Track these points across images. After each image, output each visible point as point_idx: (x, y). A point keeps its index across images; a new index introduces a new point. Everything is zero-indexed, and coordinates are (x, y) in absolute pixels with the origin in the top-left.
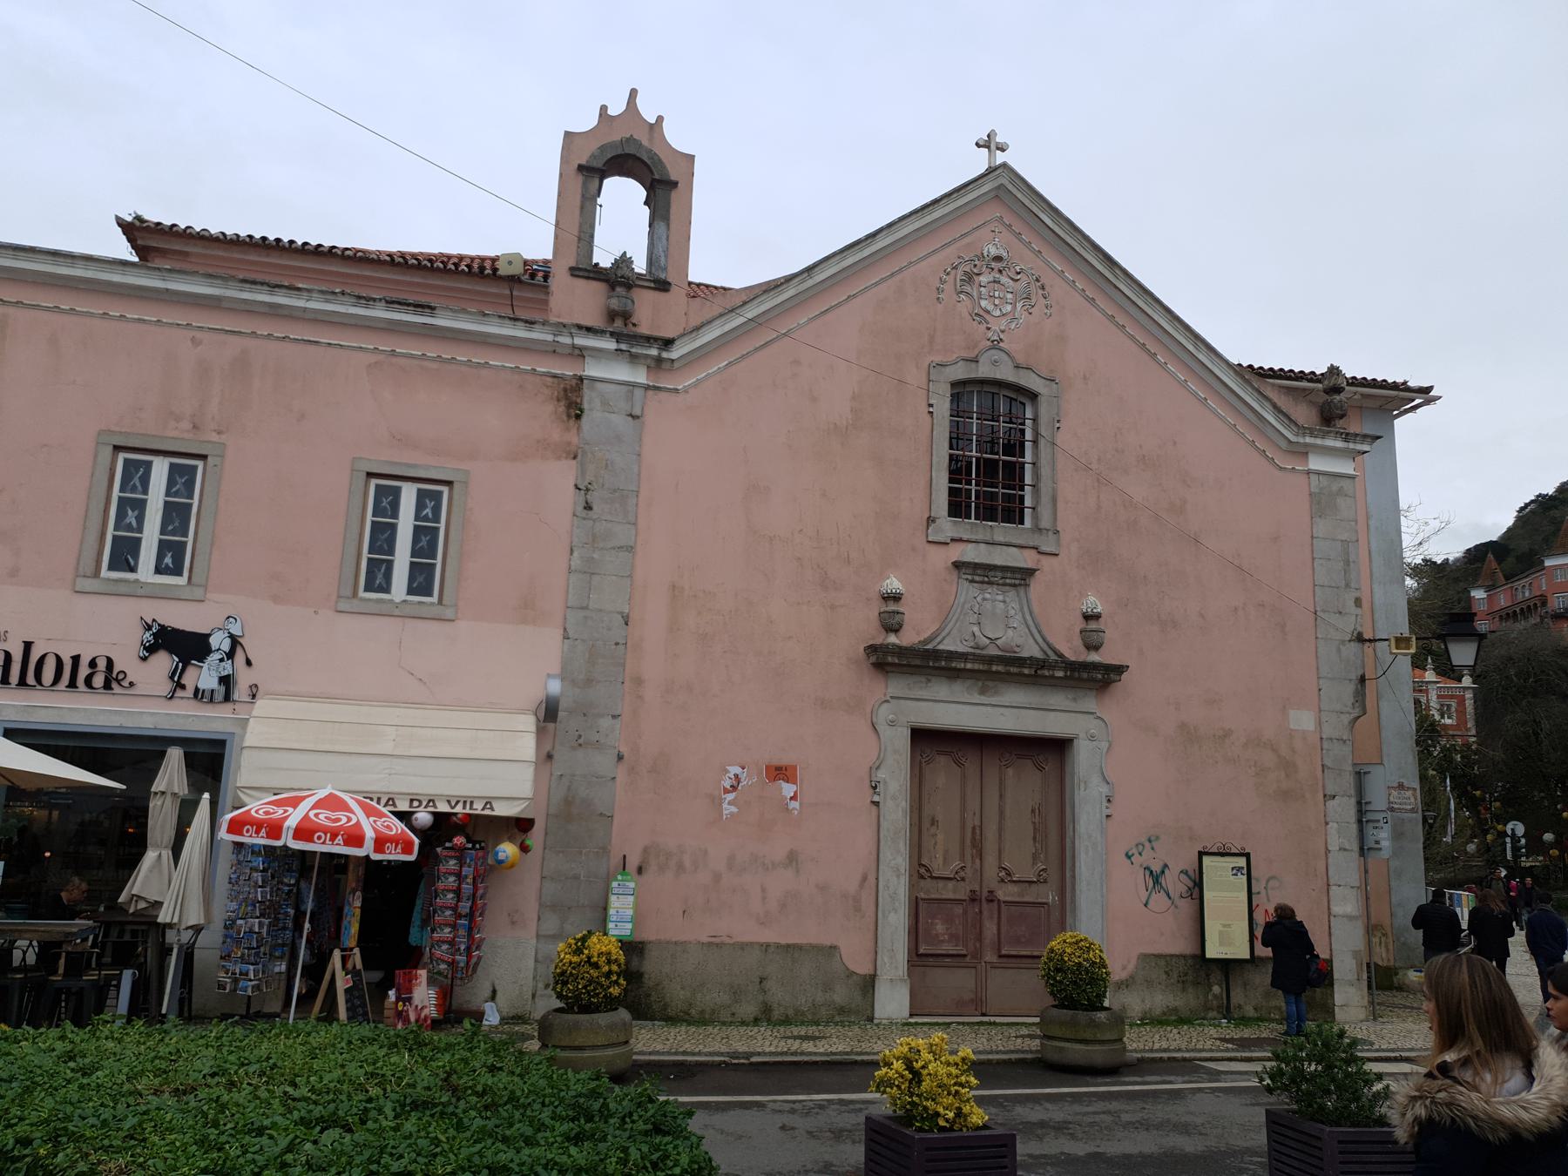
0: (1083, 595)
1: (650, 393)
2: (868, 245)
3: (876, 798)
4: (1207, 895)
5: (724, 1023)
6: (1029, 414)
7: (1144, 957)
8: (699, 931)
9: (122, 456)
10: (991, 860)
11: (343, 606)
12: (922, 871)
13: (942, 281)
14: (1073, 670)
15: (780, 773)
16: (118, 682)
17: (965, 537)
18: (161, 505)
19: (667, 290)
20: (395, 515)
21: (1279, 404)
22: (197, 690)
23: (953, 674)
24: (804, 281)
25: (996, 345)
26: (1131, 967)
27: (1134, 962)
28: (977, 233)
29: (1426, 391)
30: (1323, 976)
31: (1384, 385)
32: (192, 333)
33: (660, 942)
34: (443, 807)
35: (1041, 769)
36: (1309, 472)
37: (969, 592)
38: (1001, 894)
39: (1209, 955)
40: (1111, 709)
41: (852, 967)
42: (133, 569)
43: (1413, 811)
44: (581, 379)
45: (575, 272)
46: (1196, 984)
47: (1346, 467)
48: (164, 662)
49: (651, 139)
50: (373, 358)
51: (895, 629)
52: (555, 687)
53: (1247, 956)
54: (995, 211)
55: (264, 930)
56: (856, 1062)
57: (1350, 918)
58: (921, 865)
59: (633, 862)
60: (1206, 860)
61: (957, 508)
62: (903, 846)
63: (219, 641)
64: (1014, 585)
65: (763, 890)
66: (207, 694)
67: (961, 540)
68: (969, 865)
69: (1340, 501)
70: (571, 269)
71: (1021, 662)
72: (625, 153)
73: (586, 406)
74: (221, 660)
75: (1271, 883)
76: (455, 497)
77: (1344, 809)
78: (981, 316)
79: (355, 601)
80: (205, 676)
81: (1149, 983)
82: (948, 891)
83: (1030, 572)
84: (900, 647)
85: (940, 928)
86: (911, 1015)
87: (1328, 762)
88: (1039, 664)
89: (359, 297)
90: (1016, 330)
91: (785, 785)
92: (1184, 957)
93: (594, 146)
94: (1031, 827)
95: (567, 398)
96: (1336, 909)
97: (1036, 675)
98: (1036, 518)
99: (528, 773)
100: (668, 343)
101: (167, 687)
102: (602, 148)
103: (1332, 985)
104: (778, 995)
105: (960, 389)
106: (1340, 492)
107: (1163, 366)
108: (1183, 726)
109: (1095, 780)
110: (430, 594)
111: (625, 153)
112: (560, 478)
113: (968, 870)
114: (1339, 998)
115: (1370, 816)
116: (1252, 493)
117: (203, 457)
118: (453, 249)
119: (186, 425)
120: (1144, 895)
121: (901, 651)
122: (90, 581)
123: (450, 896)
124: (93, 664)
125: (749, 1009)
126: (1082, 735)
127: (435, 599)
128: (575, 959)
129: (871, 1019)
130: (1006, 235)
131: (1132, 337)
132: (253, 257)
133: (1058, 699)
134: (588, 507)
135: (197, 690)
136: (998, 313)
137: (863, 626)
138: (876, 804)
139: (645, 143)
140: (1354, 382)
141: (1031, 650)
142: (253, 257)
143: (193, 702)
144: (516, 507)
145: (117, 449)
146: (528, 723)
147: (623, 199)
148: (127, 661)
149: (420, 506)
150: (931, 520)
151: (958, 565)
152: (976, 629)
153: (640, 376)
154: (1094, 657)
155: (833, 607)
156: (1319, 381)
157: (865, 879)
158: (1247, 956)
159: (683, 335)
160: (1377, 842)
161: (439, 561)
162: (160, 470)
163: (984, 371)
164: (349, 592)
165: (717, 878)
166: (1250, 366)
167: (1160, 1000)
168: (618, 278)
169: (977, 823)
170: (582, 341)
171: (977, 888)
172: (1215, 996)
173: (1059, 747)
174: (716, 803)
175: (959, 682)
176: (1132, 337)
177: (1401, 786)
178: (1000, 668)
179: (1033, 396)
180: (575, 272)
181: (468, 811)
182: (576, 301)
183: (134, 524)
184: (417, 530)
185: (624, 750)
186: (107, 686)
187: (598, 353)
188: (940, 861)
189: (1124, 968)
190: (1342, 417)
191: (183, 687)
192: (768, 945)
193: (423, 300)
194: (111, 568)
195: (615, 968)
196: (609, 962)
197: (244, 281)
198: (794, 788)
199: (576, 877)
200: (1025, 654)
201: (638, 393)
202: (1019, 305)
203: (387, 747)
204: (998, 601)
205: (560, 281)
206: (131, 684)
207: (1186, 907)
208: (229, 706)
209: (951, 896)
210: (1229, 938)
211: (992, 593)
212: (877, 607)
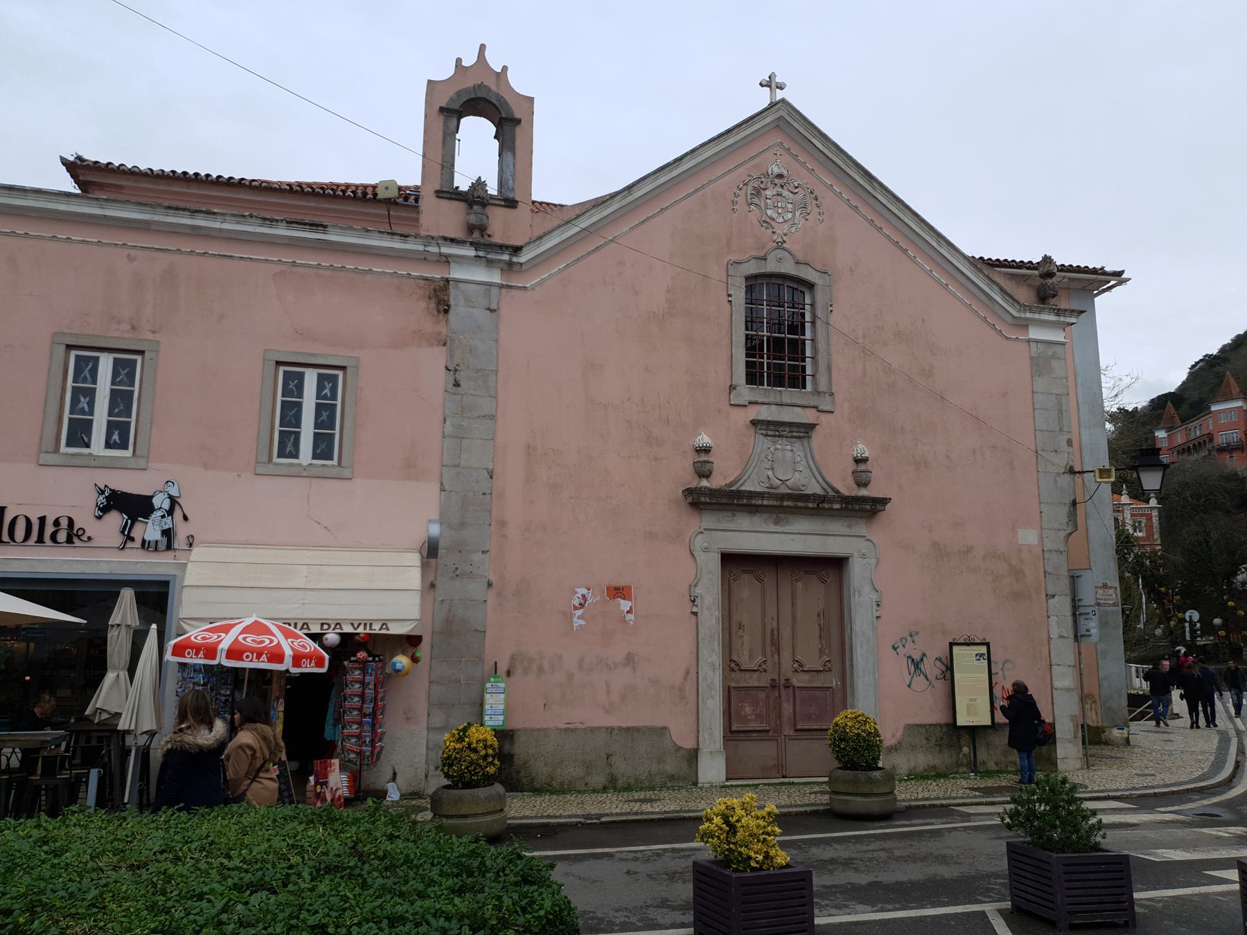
1: (504, 291)
3: (695, 610)
4: (957, 676)
5: (579, 792)
6: (808, 301)
7: (909, 727)
8: (556, 720)
12: (733, 665)
14: (847, 503)
15: (619, 592)
16: (79, 537)
17: (760, 400)
18: (108, 392)
19: (515, 207)
20: (300, 395)
22: (144, 541)
24: (625, 197)
25: (780, 246)
26: (899, 735)
27: (901, 730)
28: (763, 156)
30: (1048, 736)
31: (1086, 270)
32: (126, 252)
33: (526, 730)
34: (348, 629)
36: (1029, 341)
37: (764, 444)
38: (795, 682)
40: (878, 533)
42: (88, 446)
43: (1114, 605)
44: (447, 281)
45: (440, 194)
47: (1058, 336)
48: (115, 519)
49: (498, 85)
50: (278, 268)
51: (707, 475)
52: (435, 530)
53: (989, 723)
54: (777, 138)
56: (684, 818)
57: (1068, 690)
58: (731, 661)
60: (955, 649)
61: (753, 377)
62: (717, 646)
63: (161, 502)
65: (608, 685)
67: (756, 403)
69: (1055, 364)
70: (437, 192)
71: (805, 498)
72: (478, 97)
73: (452, 303)
76: (349, 379)
77: (1061, 605)
78: (767, 223)
79: (271, 466)
80: (151, 530)
81: (913, 747)
82: (753, 681)
83: (811, 427)
84: (710, 490)
85: (748, 709)
86: (727, 780)
87: (1049, 569)
88: (821, 499)
89: (264, 219)
90: (797, 233)
91: (622, 601)
93: (452, 92)
94: (817, 628)
95: (436, 296)
96: (1057, 684)
97: (818, 508)
98: (815, 383)
99: (416, 599)
100: (517, 250)
101: (118, 540)
102: (458, 93)
103: (1055, 742)
104: (622, 768)
105: (753, 282)
107: (913, 259)
109: (867, 589)
112: (433, 361)
113: (769, 663)
115: (1082, 610)
117: (142, 353)
119: (126, 326)
120: (907, 678)
121: (712, 492)
125: (598, 780)
126: (856, 554)
127: (335, 462)
128: (458, 746)
129: (695, 784)
130: (786, 157)
131: (888, 237)
132: (193, 190)
133: (836, 526)
134: (457, 384)
135: (144, 541)
136: (781, 220)
137: (681, 473)
138: (695, 614)
139: (493, 88)
140: (1063, 268)
141: (814, 488)
143: (141, 551)
144: (398, 387)
149: (320, 387)
150: (732, 388)
151: (754, 423)
152: (770, 473)
153: (495, 277)
154: (864, 492)
157: (687, 673)
158: (989, 723)
159: (527, 244)
160: (1088, 630)
162: (106, 364)
163: (771, 267)
164: (265, 459)
165: (570, 677)
166: (981, 258)
167: (922, 760)
169: (775, 626)
170: (446, 250)
173: (837, 564)
174: (568, 617)
176: (888, 237)
177: (1105, 586)
178: (790, 504)
179: (811, 286)
180: (440, 194)
181: (368, 631)
182: (441, 218)
183: (86, 408)
185: (493, 578)
186: (69, 540)
188: (747, 657)
189: (893, 736)
190: (1054, 296)
191: (133, 539)
192: (613, 729)
193: (317, 220)
194: (69, 444)
196: (486, 747)
197: (169, 208)
200: (809, 492)
201: (494, 291)
202: (798, 213)
203: (300, 582)
204: (786, 450)
205: (428, 202)
206: (89, 538)
207: (941, 686)
208: (171, 554)
210: (974, 708)
211: (782, 444)
212: (691, 458)
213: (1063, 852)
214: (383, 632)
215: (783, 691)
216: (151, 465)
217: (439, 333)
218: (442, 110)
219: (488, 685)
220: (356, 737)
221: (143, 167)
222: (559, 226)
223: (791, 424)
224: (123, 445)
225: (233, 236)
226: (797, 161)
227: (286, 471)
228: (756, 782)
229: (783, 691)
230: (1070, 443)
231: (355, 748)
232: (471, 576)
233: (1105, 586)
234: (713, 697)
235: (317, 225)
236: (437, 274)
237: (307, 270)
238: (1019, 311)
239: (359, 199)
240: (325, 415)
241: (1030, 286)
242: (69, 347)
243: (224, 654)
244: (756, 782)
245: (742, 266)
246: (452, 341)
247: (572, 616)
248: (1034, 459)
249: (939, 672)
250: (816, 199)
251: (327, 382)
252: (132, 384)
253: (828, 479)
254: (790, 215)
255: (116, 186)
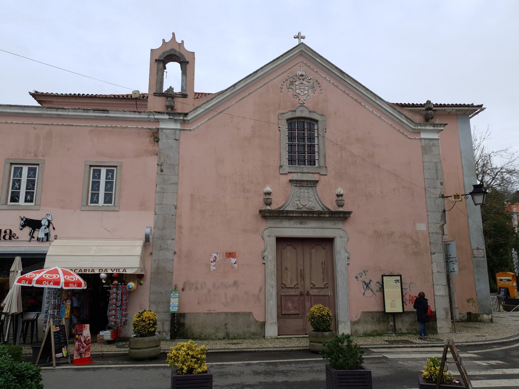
0: (336, 188)
1: (182, 132)
2: (255, 76)
3: (264, 262)
4: (385, 290)
5: (212, 340)
6: (316, 128)
7: (364, 313)
8: (203, 309)
9: (13, 166)
10: (307, 281)
11: (83, 208)
12: (283, 286)
13: (283, 85)
14: (332, 214)
15: (230, 255)
16: (13, 237)
17: (293, 171)
18: (26, 180)
19: (186, 97)
20: (99, 178)
21: (407, 115)
22: (38, 238)
23: (290, 218)
24: (232, 90)
25: (302, 105)
26: (359, 316)
27: (360, 314)
28: (295, 67)
29: (481, 106)
30: (433, 317)
31: (464, 106)
32: (33, 126)
33: (190, 313)
34: (110, 272)
35: (324, 249)
36: (421, 139)
37: (295, 190)
38: (312, 292)
39: (387, 311)
40: (348, 227)
41: (257, 319)
42: (18, 201)
43: (483, 257)
44: (158, 129)
45: (155, 94)
46: (384, 321)
47: (435, 136)
48: (27, 230)
49: (179, 49)
50: (91, 128)
51: (270, 204)
52: (148, 231)
53: (402, 311)
54: (301, 59)
55: (56, 313)
56: (244, 352)
57: (442, 296)
58: (282, 284)
59: (180, 287)
60: (385, 278)
61: (291, 161)
62: (274, 277)
63: (44, 222)
64: (311, 187)
65: (225, 295)
66: (41, 239)
67: (292, 172)
68: (300, 283)
69: (434, 149)
70: (154, 93)
71: (313, 212)
72: (171, 54)
73: (160, 138)
74: (45, 228)
75: (411, 285)
76: (118, 171)
77: (439, 258)
78: (296, 96)
79: (87, 207)
80: (40, 233)
81: (366, 322)
82: (292, 292)
83: (317, 182)
84: (272, 210)
85: (290, 305)
86: (279, 335)
87: (432, 241)
88: (319, 213)
89: (84, 110)
90: (306, 100)
91: (232, 259)
92: (379, 312)
93: (160, 53)
94: (322, 269)
95: (154, 135)
96: (436, 293)
97: (319, 217)
98: (319, 163)
99: (138, 259)
100: (186, 115)
101: (28, 238)
102: (163, 53)
103: (436, 320)
104: (232, 330)
105: (290, 121)
106: (434, 145)
107: (364, 106)
108: (375, 231)
109: (343, 252)
110: (111, 203)
111: (171, 54)
112: (152, 162)
113: (299, 285)
114: (439, 325)
115: (451, 260)
116: (400, 149)
117: (116, 167)
118: (103, 93)
119: (33, 155)
120: (363, 291)
121: (270, 211)
122: (3, 206)
123: (114, 300)
124: (5, 232)
125: (221, 334)
126: (338, 236)
127: (113, 204)
128: (138, 319)
129: (264, 337)
130: (305, 67)
131: (352, 98)
132: (79, 100)
133: (328, 224)
134: (162, 171)
135: (38, 238)
136: (303, 94)
137: (258, 203)
138: (264, 264)
139: (178, 50)
140: (436, 105)
141: (318, 208)
142: (71, 100)
143: (37, 242)
144: (138, 172)
145: (12, 164)
146: (141, 243)
147: (173, 69)
148: (16, 230)
149: (107, 175)
150: (281, 166)
151: (291, 181)
152: (298, 202)
153: (178, 126)
154: (341, 209)
155: (247, 198)
156: (424, 107)
157: (261, 289)
158: (402, 311)
159: (191, 111)
160: (454, 269)
161: (114, 192)
162: (25, 170)
163: (298, 114)
164: (85, 204)
165: (209, 291)
166: (397, 104)
167: (370, 328)
168: (170, 95)
169: (302, 268)
170: (157, 117)
171: (302, 290)
172: (391, 326)
173: (330, 241)
174: (209, 266)
175: (292, 220)
176: (352, 98)
177: (478, 249)
178: (306, 215)
179: (317, 121)
180: (155, 94)
181: (118, 272)
182: (157, 104)
183: (18, 187)
184: (106, 182)
185: (176, 250)
186: (10, 238)
187: (164, 120)
188: (289, 282)
189: (356, 317)
190: (432, 118)
191: (34, 237)
192: (228, 313)
193: (104, 108)
194: (11, 201)
195: (151, 322)
196: (149, 320)
197: (48, 108)
198: (235, 260)
199: (161, 293)
200: (316, 210)
201: (178, 132)
202: (310, 91)
203: (92, 253)
204: (305, 192)
205: (151, 98)
206: (17, 237)
207: (379, 294)
208: (48, 243)
209: (293, 294)
210: (393, 305)
211: (303, 190)
212: (263, 197)
213: (340, 369)
214: (124, 273)
215: (306, 296)
216: (41, 208)
217: (155, 150)
218: (156, 60)
219: (172, 294)
220: (114, 315)
221: (59, 93)
222: (204, 104)
223: (307, 181)
224: (31, 201)
225: (73, 117)
226: (310, 68)
227: (93, 209)
228: (291, 336)
229: (306, 296)
230: (442, 184)
231: (114, 320)
232: (167, 249)
233: (478, 249)
234: (272, 300)
235: (105, 110)
236: (154, 126)
237: (102, 128)
238: (415, 126)
239: (129, 98)
240: (109, 186)
241: (421, 114)
242: (12, 164)
243: (35, 282)
244: (291, 336)
245: (285, 115)
246: (160, 153)
247: (210, 265)
248: (424, 192)
249: (378, 288)
250: (319, 84)
251: (110, 173)
252: (35, 177)
253: (325, 204)
254: (307, 92)
255: (50, 101)
